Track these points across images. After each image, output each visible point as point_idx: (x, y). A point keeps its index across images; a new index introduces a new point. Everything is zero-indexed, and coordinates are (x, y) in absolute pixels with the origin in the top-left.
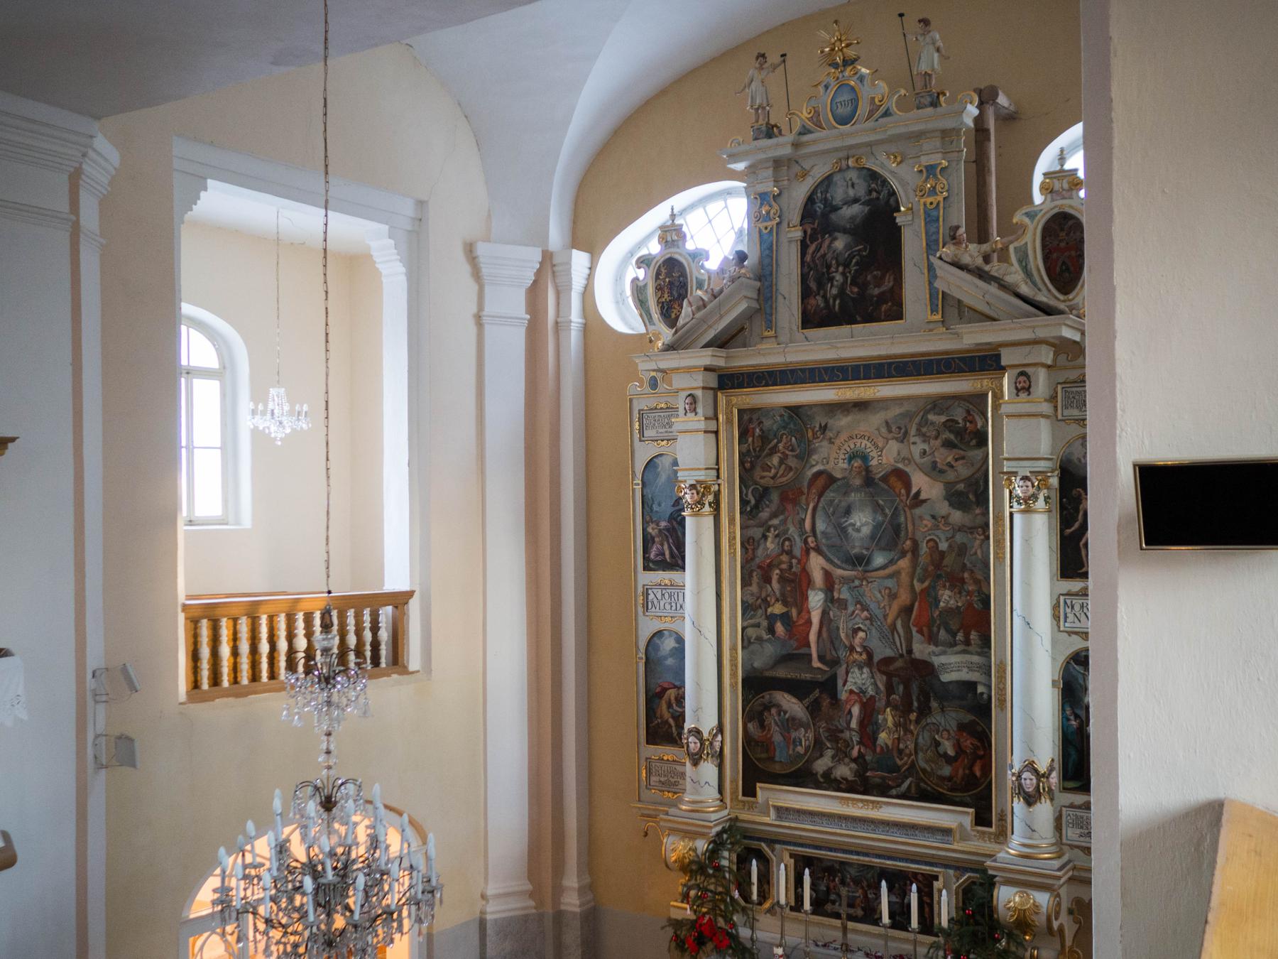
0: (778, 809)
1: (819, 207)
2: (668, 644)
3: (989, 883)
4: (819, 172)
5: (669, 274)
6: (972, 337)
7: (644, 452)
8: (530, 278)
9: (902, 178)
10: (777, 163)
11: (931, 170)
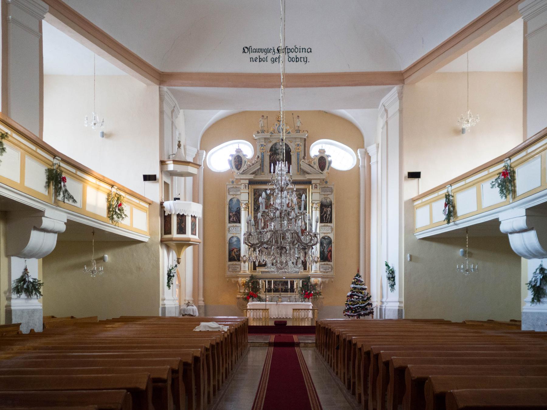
0: (261, 272)
1: (274, 149)
2: (235, 239)
3: (309, 278)
4: (274, 142)
5: (238, 158)
6: (308, 177)
7: (229, 197)
8: (194, 156)
9: (292, 146)
10: (265, 139)
11: (298, 145)
